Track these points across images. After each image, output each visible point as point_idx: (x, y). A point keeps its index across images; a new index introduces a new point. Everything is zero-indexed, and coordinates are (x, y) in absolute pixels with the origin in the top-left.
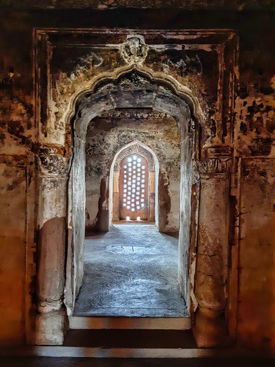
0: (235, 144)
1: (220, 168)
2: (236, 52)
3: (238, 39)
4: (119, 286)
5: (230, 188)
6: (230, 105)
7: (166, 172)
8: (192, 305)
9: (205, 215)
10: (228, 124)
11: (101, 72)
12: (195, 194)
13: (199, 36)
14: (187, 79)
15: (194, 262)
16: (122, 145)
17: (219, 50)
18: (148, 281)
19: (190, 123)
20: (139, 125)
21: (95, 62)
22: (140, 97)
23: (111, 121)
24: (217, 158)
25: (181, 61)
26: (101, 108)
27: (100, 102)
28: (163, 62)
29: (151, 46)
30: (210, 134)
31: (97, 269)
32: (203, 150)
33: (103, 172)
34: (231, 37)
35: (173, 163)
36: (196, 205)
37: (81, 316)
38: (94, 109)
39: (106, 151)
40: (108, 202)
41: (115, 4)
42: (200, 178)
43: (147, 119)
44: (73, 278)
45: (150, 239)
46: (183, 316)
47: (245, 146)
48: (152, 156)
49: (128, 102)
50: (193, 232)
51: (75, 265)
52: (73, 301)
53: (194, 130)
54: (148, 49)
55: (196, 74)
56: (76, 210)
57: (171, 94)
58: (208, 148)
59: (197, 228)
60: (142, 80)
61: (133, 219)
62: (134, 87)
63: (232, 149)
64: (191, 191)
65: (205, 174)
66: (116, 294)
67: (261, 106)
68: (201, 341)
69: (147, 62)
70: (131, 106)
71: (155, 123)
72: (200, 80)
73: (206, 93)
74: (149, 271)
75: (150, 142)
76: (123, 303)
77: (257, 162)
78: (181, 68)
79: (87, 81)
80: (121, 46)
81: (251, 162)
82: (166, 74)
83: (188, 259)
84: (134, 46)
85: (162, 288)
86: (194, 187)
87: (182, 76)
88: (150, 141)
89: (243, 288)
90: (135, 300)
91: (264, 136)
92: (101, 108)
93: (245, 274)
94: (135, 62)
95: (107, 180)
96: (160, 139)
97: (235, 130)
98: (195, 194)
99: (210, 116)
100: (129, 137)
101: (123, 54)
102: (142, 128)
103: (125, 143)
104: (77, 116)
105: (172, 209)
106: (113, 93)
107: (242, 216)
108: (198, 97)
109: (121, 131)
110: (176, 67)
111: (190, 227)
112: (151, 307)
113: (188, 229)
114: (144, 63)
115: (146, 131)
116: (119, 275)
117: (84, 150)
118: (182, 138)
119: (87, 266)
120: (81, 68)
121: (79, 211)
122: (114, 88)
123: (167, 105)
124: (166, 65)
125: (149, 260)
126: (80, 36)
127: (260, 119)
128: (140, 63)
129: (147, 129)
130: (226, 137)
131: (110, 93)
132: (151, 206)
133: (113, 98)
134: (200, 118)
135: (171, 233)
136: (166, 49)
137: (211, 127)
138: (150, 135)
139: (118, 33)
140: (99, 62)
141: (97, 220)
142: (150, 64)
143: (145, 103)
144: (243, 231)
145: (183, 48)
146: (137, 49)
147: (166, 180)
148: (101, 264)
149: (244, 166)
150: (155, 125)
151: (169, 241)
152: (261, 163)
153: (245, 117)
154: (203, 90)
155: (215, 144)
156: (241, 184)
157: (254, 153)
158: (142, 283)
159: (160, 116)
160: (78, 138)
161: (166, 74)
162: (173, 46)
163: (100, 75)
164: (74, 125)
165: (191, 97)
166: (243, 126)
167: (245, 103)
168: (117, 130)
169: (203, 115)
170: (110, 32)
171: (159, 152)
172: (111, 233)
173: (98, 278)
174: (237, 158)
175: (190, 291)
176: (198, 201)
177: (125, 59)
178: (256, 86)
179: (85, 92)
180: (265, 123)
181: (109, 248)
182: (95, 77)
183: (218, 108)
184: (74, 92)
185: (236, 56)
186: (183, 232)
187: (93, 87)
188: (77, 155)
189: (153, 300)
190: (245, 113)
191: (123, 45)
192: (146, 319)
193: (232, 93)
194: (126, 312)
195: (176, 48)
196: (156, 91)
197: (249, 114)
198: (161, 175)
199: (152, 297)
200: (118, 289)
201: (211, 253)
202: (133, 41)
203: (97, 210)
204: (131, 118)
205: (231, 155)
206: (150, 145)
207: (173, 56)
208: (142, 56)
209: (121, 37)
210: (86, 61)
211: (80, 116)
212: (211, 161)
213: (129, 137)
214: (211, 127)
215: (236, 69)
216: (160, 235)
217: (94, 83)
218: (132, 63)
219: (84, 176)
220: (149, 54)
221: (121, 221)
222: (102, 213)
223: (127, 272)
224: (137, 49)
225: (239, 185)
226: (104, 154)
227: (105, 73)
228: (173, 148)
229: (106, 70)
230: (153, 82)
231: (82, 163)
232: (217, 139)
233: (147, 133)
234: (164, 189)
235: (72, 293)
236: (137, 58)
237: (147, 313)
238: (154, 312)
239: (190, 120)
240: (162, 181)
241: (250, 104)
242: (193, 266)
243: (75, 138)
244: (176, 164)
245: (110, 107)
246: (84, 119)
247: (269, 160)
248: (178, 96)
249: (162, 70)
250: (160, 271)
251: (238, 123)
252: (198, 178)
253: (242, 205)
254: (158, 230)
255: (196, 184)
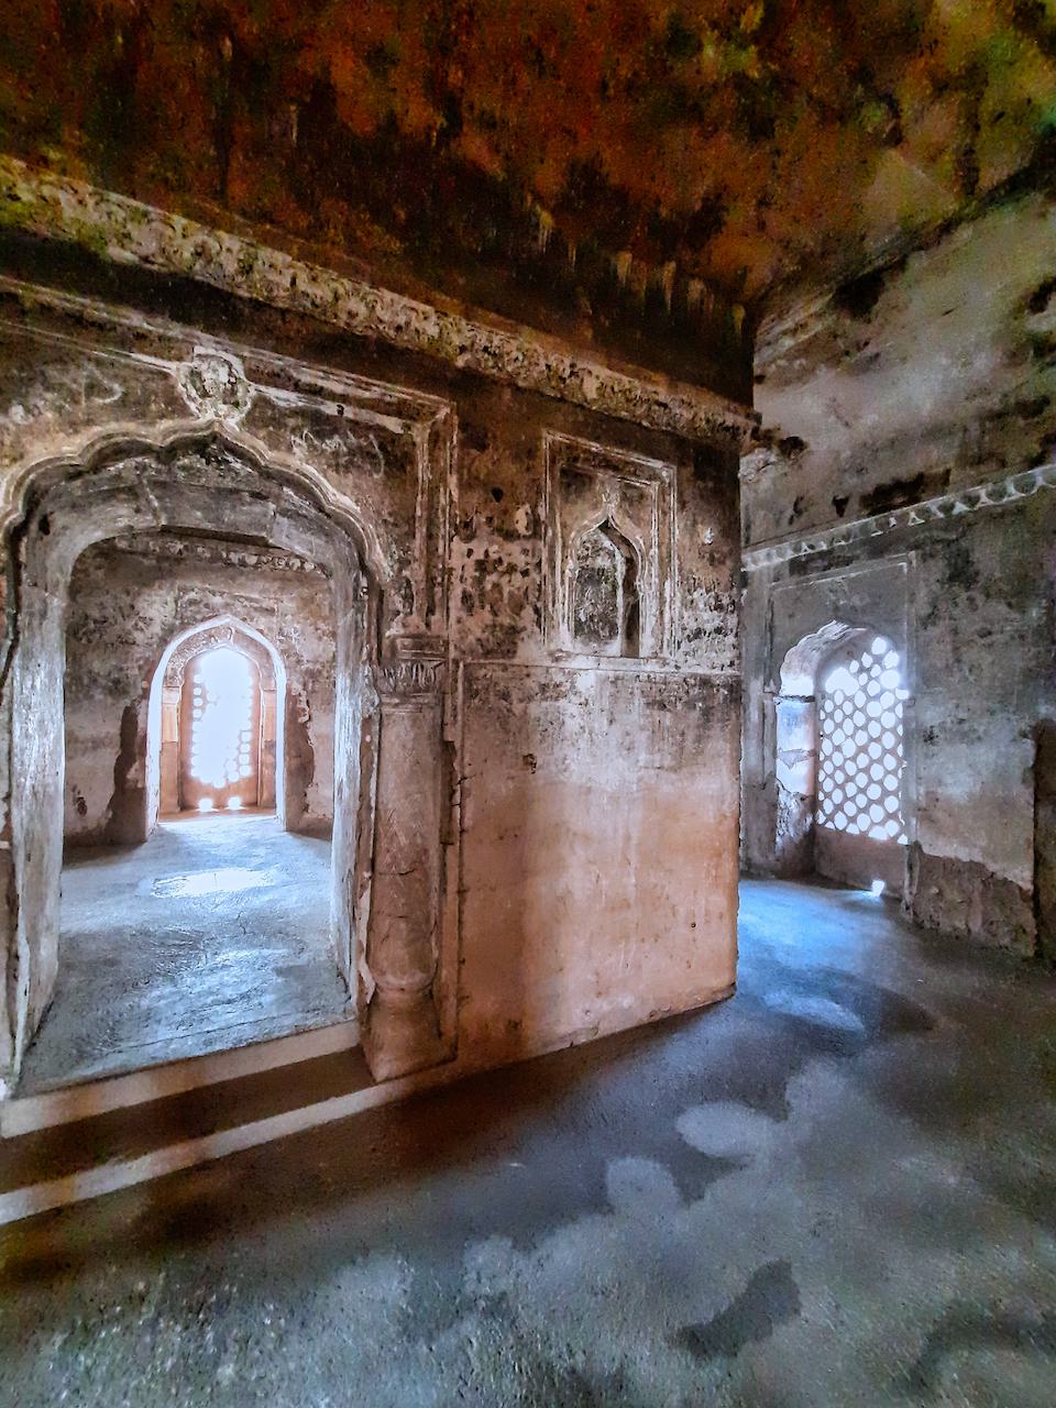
0: (452, 633)
1: (422, 681)
2: (452, 448)
3: (456, 419)
4: (172, 979)
5: (443, 725)
6: (441, 551)
7: (304, 693)
8: (362, 991)
9: (391, 785)
10: (438, 590)
11: (117, 420)
12: (368, 739)
13: (375, 396)
14: (350, 479)
15: (367, 893)
16: (189, 624)
17: (420, 433)
18: (255, 952)
19: (357, 580)
20: (233, 579)
21: (93, 388)
22: (234, 507)
23: (154, 562)
24: (417, 663)
25: (337, 438)
26: (119, 518)
27: (114, 502)
28: (293, 431)
29: (262, 388)
30: (400, 607)
31: (106, 947)
32: (386, 642)
33: (132, 690)
34: (441, 415)
35: (320, 672)
36: (372, 763)
37: (44, 1093)
38: (95, 517)
39: (139, 636)
40: (143, 766)
41: (161, 260)
42: (381, 704)
43: (255, 566)
44: (14, 989)
45: (261, 851)
46: (341, 1019)
47: (471, 638)
48: (268, 654)
49: (199, 514)
50: (365, 826)
51: (24, 950)
52: (14, 1055)
53: (366, 597)
54: (253, 393)
55: (371, 475)
56: (28, 792)
57: (314, 511)
58: (395, 637)
59: (373, 816)
60: (238, 466)
61: (220, 806)
62: (211, 476)
63: (447, 643)
64: (359, 733)
65: (391, 695)
66: (162, 1002)
67: (500, 561)
68: (384, 1066)
69: (251, 422)
70: (209, 526)
71: (274, 580)
72: (380, 488)
73: (391, 520)
74: (254, 928)
75: (262, 622)
76: (182, 1023)
77: (491, 670)
78: (336, 454)
79: (68, 435)
80: (178, 369)
81: (483, 672)
82: (298, 459)
83: (354, 888)
84: (214, 377)
85: (291, 964)
86: (367, 722)
87: (337, 472)
88: (263, 620)
89: (470, 932)
90: (218, 1008)
91: (507, 621)
92: (119, 518)
93: (472, 903)
94: (217, 415)
95: (141, 711)
96: (289, 617)
97: (451, 604)
98: (368, 739)
99: (400, 570)
100: (207, 606)
101: (183, 388)
102: (241, 586)
103: (195, 620)
104: (34, 527)
105: (318, 776)
106: (157, 484)
107: (466, 783)
108: (376, 526)
109: (185, 590)
110: (323, 451)
111: (359, 815)
112: (261, 1017)
113: (353, 819)
114: (242, 424)
115: (253, 596)
116: (174, 951)
117: (60, 626)
118: (340, 615)
119: (71, 947)
120: (49, 396)
121: (40, 796)
122: (159, 471)
123: (303, 536)
124: (298, 440)
125: (258, 902)
126: (46, 309)
127: (496, 586)
128: (232, 423)
129: (256, 591)
130: (433, 619)
131: (145, 482)
132: (266, 772)
133: (157, 498)
134: (379, 571)
135: (312, 829)
136: (300, 404)
137: (403, 592)
138: (264, 606)
139: (170, 334)
140: (109, 392)
141: (110, 814)
142: (258, 428)
143: (250, 525)
144: (470, 813)
145: (341, 412)
146: (222, 387)
147: (304, 710)
148: (119, 931)
149: (469, 679)
150: (277, 585)
151: (651, 1164)
152: (500, 673)
153: (470, 581)
154: (385, 513)
155: (412, 630)
156: (464, 715)
157: (488, 653)
158: (239, 962)
159: (287, 564)
160: (36, 590)
161: (298, 459)
162: (316, 402)
163: (113, 427)
164: (23, 549)
165: (358, 521)
166: (466, 597)
167: (470, 552)
168: (172, 585)
169: (385, 565)
170: (145, 325)
171: (284, 646)
172: (154, 844)
173: (101, 971)
174: (456, 662)
175: (358, 959)
176: (376, 754)
177: (188, 403)
178: (490, 520)
179: (58, 463)
180: (506, 595)
181: (147, 885)
182: (96, 429)
183: (417, 554)
184: (22, 457)
185: (451, 455)
186: (342, 828)
187: (89, 455)
188: (33, 636)
189: (267, 999)
190: (471, 572)
191: (185, 366)
192: (251, 1050)
193: (444, 530)
194: (191, 1047)
195: (322, 408)
196: (277, 499)
197: (477, 574)
198: (291, 699)
199: (263, 992)
200: (169, 989)
201: (404, 867)
202: (213, 363)
203: (110, 791)
204: (213, 560)
205: (445, 656)
206: (262, 627)
207: (322, 426)
208: (237, 404)
209: (177, 345)
210: (66, 380)
211: (45, 527)
212: (403, 665)
213: (207, 606)
214: (403, 592)
215: (453, 480)
216: (289, 837)
217: (92, 445)
218: (209, 416)
219: (59, 696)
220: (255, 405)
221: (185, 813)
222: (128, 797)
223: (196, 941)
224: (222, 387)
225: (459, 718)
226: (134, 643)
227: (131, 426)
228: (320, 639)
229: (135, 417)
230: (266, 474)
231: (50, 661)
232: (416, 620)
233: (257, 601)
234: (297, 730)
235: (9, 1036)
236: (225, 407)
237: (249, 1033)
238: (268, 1026)
239: (357, 577)
240: (293, 713)
241: (479, 555)
242: (365, 902)
243: (24, 588)
244: (325, 674)
245: (144, 522)
246: (63, 541)
247: (514, 669)
248: (328, 516)
249: (290, 448)
250: (287, 924)
251: (457, 591)
252: (377, 702)
253: (467, 760)
254: (283, 827)
255: (370, 717)
